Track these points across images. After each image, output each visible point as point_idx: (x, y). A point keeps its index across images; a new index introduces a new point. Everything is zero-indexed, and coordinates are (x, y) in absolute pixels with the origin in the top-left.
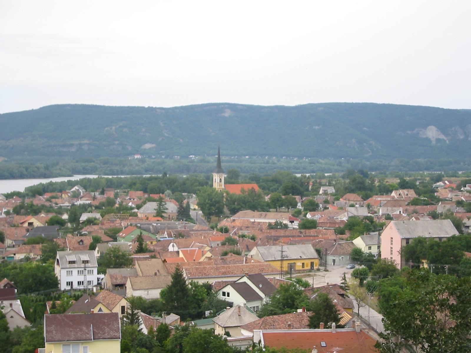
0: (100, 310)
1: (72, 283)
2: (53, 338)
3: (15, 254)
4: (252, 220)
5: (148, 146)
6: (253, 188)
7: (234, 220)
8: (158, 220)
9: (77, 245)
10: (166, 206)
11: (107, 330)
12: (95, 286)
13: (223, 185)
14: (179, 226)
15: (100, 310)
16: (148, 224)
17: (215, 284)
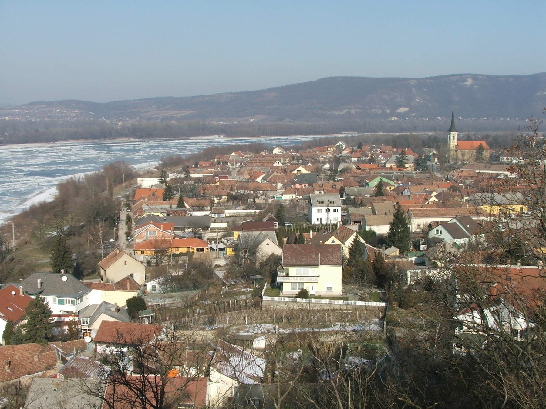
0: (333, 242)
1: (321, 219)
2: (288, 262)
3: (282, 195)
4: (478, 171)
5: (402, 110)
6: (481, 144)
7: (462, 171)
8: (400, 170)
9: (331, 189)
10: (408, 158)
11: (331, 258)
12: (339, 222)
13: (456, 142)
14: (415, 175)
15: (333, 242)
16: (390, 173)
17: (433, 224)
